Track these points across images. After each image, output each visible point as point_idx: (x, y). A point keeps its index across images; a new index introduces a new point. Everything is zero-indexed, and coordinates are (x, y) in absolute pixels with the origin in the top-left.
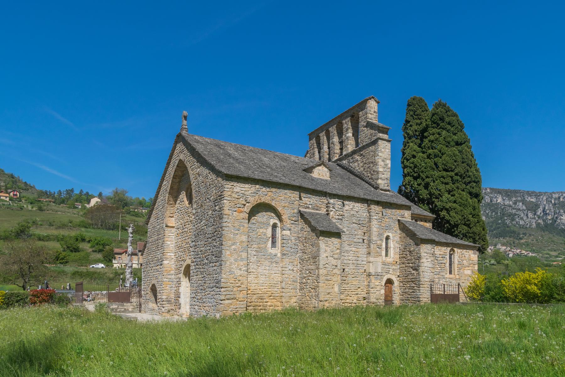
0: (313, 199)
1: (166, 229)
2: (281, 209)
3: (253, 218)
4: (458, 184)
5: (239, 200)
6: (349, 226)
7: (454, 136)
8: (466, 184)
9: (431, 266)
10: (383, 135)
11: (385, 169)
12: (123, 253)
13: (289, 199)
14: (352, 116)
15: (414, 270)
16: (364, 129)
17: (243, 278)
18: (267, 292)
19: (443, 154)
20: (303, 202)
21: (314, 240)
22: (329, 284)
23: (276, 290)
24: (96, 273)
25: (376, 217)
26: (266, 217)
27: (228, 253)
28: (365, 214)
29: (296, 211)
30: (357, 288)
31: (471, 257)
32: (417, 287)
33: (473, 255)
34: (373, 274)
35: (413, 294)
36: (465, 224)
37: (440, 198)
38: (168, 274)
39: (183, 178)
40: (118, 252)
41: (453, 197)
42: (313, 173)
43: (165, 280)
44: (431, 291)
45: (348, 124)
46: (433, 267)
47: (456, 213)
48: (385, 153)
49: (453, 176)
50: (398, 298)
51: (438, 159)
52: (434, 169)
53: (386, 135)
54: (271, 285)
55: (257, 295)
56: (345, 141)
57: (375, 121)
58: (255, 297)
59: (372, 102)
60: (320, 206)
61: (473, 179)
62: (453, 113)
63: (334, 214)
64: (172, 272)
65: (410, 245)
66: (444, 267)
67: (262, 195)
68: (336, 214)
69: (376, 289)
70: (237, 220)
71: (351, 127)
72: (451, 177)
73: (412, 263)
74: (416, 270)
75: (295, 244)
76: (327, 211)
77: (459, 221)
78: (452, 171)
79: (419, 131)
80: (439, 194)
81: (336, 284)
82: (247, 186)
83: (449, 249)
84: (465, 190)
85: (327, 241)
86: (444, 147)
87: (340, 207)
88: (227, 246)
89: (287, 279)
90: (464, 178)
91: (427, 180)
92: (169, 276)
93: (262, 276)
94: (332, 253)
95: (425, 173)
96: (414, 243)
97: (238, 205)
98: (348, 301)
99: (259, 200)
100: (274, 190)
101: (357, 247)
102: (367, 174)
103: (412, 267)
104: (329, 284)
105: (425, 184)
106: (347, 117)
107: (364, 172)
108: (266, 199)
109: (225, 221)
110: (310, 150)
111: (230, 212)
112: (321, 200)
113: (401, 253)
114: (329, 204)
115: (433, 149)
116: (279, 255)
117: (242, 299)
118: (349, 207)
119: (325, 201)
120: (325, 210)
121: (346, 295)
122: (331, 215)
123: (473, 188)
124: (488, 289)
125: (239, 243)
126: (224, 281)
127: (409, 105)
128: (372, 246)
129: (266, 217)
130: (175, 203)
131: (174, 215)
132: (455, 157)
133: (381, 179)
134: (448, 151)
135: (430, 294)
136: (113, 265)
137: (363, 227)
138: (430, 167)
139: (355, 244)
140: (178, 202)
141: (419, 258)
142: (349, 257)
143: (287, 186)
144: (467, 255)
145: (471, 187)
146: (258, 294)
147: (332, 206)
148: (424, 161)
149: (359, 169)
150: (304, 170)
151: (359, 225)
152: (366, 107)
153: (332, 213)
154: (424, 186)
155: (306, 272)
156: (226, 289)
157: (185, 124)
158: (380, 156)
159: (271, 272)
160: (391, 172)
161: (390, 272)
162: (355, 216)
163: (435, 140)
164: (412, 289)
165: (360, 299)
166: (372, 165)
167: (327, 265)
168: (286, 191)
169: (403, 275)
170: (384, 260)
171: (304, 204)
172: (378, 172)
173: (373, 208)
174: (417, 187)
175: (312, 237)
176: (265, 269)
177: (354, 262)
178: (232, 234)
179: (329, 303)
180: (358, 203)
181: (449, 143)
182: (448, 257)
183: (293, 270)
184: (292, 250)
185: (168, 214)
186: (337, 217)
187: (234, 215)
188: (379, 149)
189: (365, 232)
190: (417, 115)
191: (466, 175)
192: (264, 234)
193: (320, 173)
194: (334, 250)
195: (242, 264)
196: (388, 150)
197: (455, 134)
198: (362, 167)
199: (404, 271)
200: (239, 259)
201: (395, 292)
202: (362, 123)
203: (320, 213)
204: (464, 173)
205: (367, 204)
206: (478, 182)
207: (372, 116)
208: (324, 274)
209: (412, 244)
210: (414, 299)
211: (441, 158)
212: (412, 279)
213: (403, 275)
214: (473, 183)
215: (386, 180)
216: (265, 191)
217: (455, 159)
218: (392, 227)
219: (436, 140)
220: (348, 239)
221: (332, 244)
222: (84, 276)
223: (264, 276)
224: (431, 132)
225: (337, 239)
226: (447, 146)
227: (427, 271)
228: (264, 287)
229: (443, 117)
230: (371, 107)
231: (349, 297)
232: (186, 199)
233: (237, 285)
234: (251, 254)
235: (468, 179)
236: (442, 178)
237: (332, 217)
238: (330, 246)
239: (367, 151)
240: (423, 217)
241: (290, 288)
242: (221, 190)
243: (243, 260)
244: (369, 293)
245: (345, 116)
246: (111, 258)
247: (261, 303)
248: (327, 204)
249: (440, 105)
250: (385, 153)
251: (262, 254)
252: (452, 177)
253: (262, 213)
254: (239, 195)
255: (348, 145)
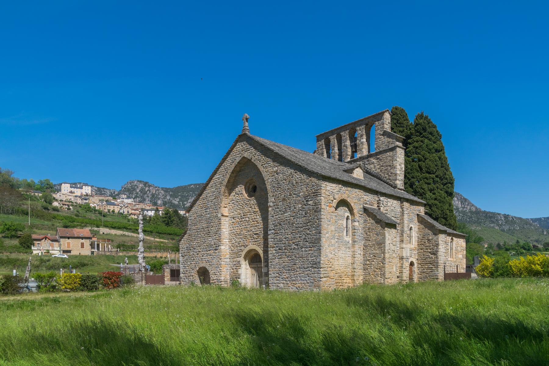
1: (222, 218)
8: (444, 185)
9: (444, 251)
12: (42, 239)
14: (367, 125)
15: (432, 254)
16: (380, 137)
21: (379, 230)
24: (18, 260)
28: (399, 209)
29: (362, 206)
32: (435, 267)
35: (431, 273)
38: (225, 258)
39: (240, 173)
40: (36, 238)
41: (434, 195)
42: (354, 174)
43: (223, 263)
45: (363, 131)
47: (437, 208)
48: (401, 158)
56: (359, 146)
57: (389, 130)
60: (374, 202)
61: (449, 181)
64: (228, 256)
67: (343, 193)
71: (365, 134)
73: (430, 249)
78: (434, 174)
86: (427, 153)
92: (225, 260)
96: (432, 233)
100: (349, 189)
102: (384, 175)
103: (430, 252)
106: (361, 125)
107: (381, 173)
108: (344, 197)
110: (318, 150)
113: (419, 241)
115: (417, 154)
116: (351, 242)
119: (377, 198)
123: (449, 188)
124: (497, 269)
128: (404, 235)
130: (230, 195)
131: (228, 205)
135: (443, 273)
136: (32, 252)
138: (416, 169)
140: (233, 194)
141: (437, 245)
145: (447, 187)
148: (409, 164)
149: (376, 170)
150: (343, 171)
152: (383, 118)
153: (382, 208)
154: (409, 185)
155: (370, 256)
157: (247, 125)
158: (398, 161)
164: (430, 269)
166: (389, 168)
168: (356, 190)
169: (421, 259)
172: (396, 174)
175: (377, 228)
180: (395, 200)
185: (223, 205)
187: (327, 209)
188: (397, 155)
190: (400, 124)
191: (444, 177)
197: (435, 143)
198: (378, 169)
199: (423, 255)
201: (415, 272)
205: (400, 201)
207: (387, 126)
209: (430, 234)
210: (432, 277)
212: (430, 261)
213: (421, 259)
216: (344, 189)
218: (414, 219)
222: (6, 263)
223: (342, 259)
224: (415, 139)
226: (429, 153)
229: (425, 127)
230: (387, 119)
232: (244, 192)
235: (445, 180)
238: (391, 235)
239: (384, 156)
241: (359, 268)
242: (319, 187)
244: (401, 273)
245: (359, 124)
246: (29, 245)
248: (378, 201)
249: (421, 116)
250: (401, 158)
252: (433, 179)
255: (362, 149)
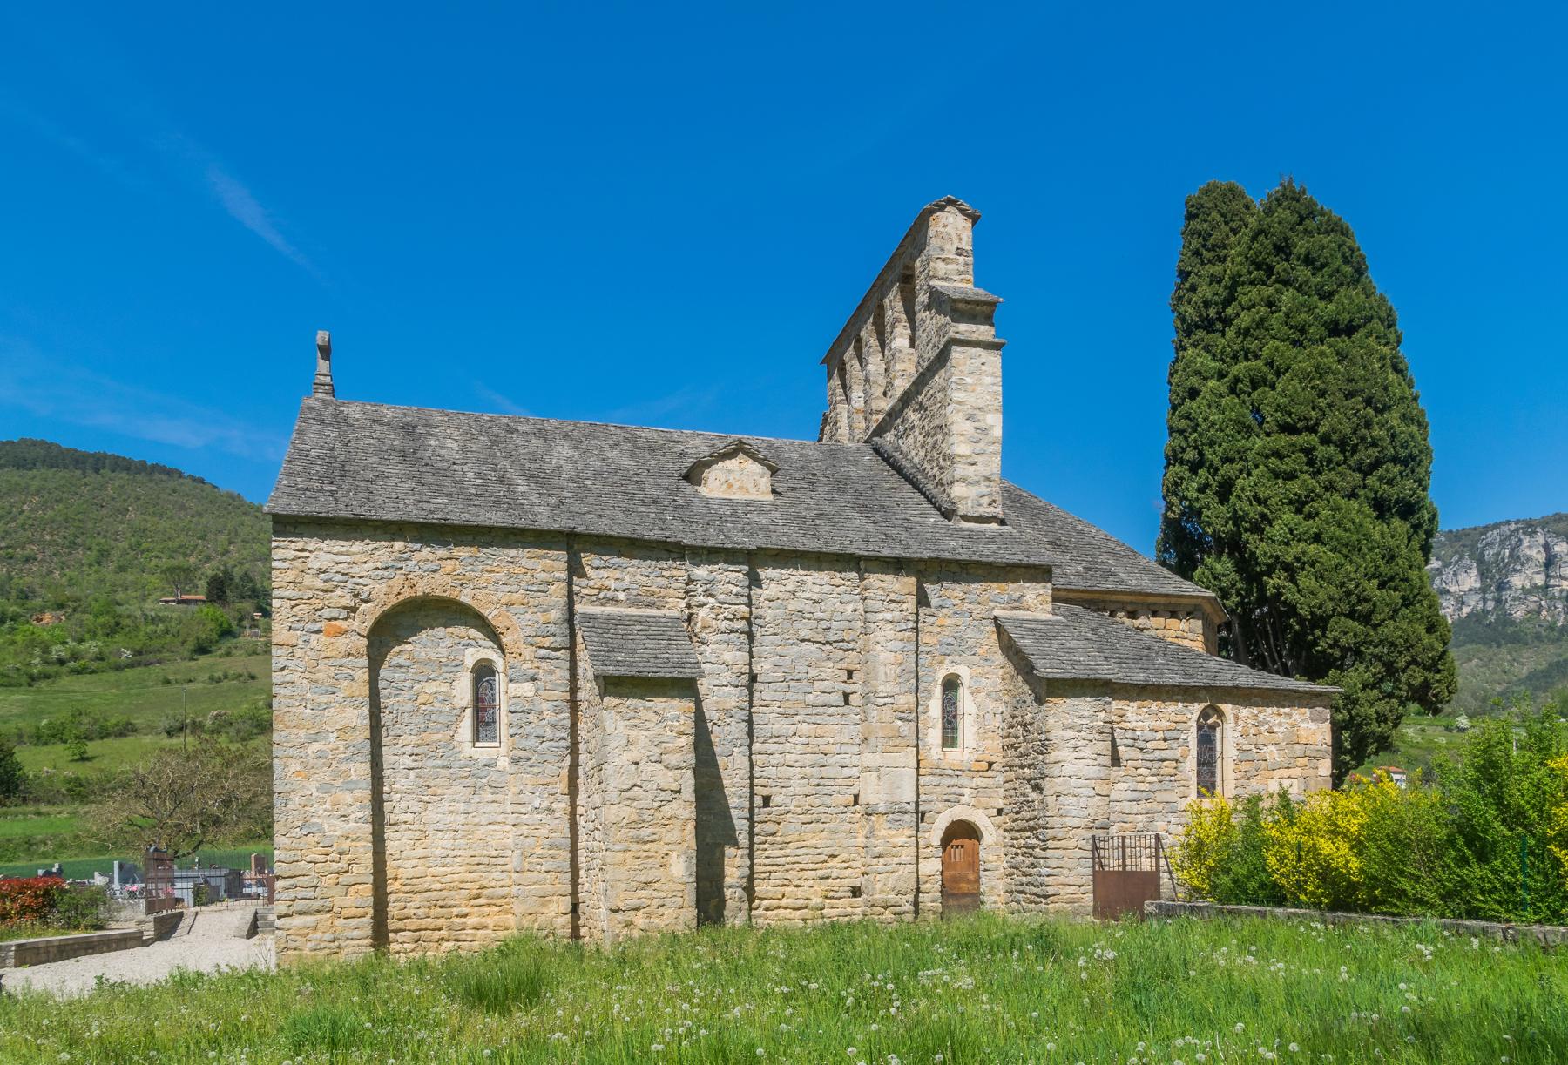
0: (632, 570)
2: (496, 612)
3: (397, 649)
4: (1332, 476)
5: (330, 594)
6: (784, 653)
7: (1321, 305)
10: (974, 327)
11: (982, 445)
13: (528, 577)
17: (354, 843)
18: (462, 885)
19: (1278, 374)
20: (591, 583)
22: (645, 854)
23: (496, 875)
25: (889, 616)
26: (448, 642)
27: (295, 766)
30: (824, 858)
31: (1302, 733)
33: (1311, 725)
34: (880, 810)
36: (1352, 615)
37: (1267, 528)
44: (1093, 858)
46: (1102, 775)
47: (1319, 576)
48: (979, 389)
49: (1314, 449)
50: (1001, 886)
51: (1264, 392)
52: (1249, 429)
53: (983, 328)
54: (476, 860)
55: (426, 894)
58: (418, 900)
59: (951, 219)
62: (1329, 220)
63: (713, 616)
65: (1025, 702)
66: (1173, 772)
67: (420, 572)
68: (721, 616)
69: (896, 860)
70: (326, 661)
72: (1303, 450)
74: (1037, 788)
75: (554, 726)
76: (689, 606)
77: (1330, 605)
79: (1216, 304)
80: (1263, 516)
81: (675, 854)
82: (358, 546)
83: (1197, 708)
84: (1361, 492)
85: (635, 710)
87: (736, 589)
88: (290, 745)
89: (528, 840)
90: (1354, 451)
91: (1226, 469)
93: (440, 833)
94: (657, 751)
95: (1220, 445)
97: (326, 613)
98: (790, 900)
99: (406, 589)
100: (463, 551)
101: (819, 719)
104: (645, 854)
105: (1221, 485)
109: (280, 665)
111: (296, 638)
112: (664, 573)
114: (693, 581)
116: (504, 763)
117: (354, 911)
118: (782, 588)
120: (683, 604)
121: (778, 882)
122: (700, 618)
123: (1390, 482)
125: (335, 735)
126: (282, 857)
127: (1190, 217)
128: (874, 713)
129: (448, 642)
132: (1320, 377)
133: (963, 480)
134: (1303, 361)
135: (1090, 871)
137: (845, 651)
139: (809, 711)
141: (1044, 747)
142: (788, 756)
143: (515, 535)
144: (1280, 725)
145: (1381, 479)
146: (429, 891)
147: (705, 587)
151: (828, 647)
153: (702, 613)
156: (292, 881)
158: (960, 403)
159: (476, 820)
160: (1006, 455)
161: (964, 800)
162: (809, 616)
163: (1254, 325)
165: (838, 895)
167: (636, 792)
168: (513, 552)
170: (936, 757)
171: (596, 591)
173: (877, 584)
174: (1197, 499)
176: (452, 812)
177: (808, 770)
178: (309, 706)
179: (649, 916)
181: (1303, 331)
182: (1192, 737)
183: (550, 810)
184: (544, 745)
186: (725, 625)
187: (313, 644)
189: (852, 667)
191: (1363, 439)
192: (440, 697)
193: (731, 480)
194: (665, 739)
195: (350, 800)
196: (989, 380)
197: (1327, 296)
200: (339, 783)
201: (988, 866)
202: (922, 298)
203: (654, 617)
204: (1354, 432)
205: (858, 571)
206: (1410, 461)
208: (625, 821)
209: (1029, 701)
211: (1273, 387)
214: (1390, 465)
215: (983, 484)
216: (431, 557)
217: (1323, 386)
219: (1258, 325)
220: (779, 696)
221: (655, 718)
225: (676, 702)
226: (1295, 343)
227: (1077, 791)
228: (449, 870)
229: (1286, 239)
231: (791, 889)
233: (335, 866)
234: (395, 766)
236: (1272, 460)
237: (704, 628)
238: (648, 725)
240: (1162, 600)
241: (543, 868)
243: (353, 786)
247: (442, 920)
249: (1289, 196)
251: (438, 762)
252: (1308, 452)
253: (431, 632)
254: (331, 580)
